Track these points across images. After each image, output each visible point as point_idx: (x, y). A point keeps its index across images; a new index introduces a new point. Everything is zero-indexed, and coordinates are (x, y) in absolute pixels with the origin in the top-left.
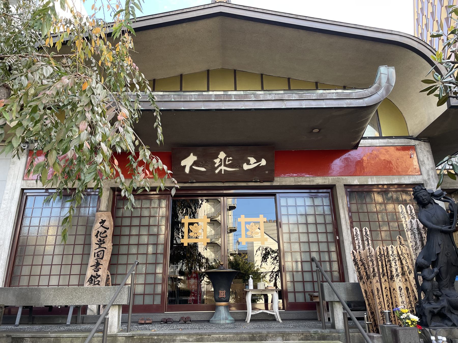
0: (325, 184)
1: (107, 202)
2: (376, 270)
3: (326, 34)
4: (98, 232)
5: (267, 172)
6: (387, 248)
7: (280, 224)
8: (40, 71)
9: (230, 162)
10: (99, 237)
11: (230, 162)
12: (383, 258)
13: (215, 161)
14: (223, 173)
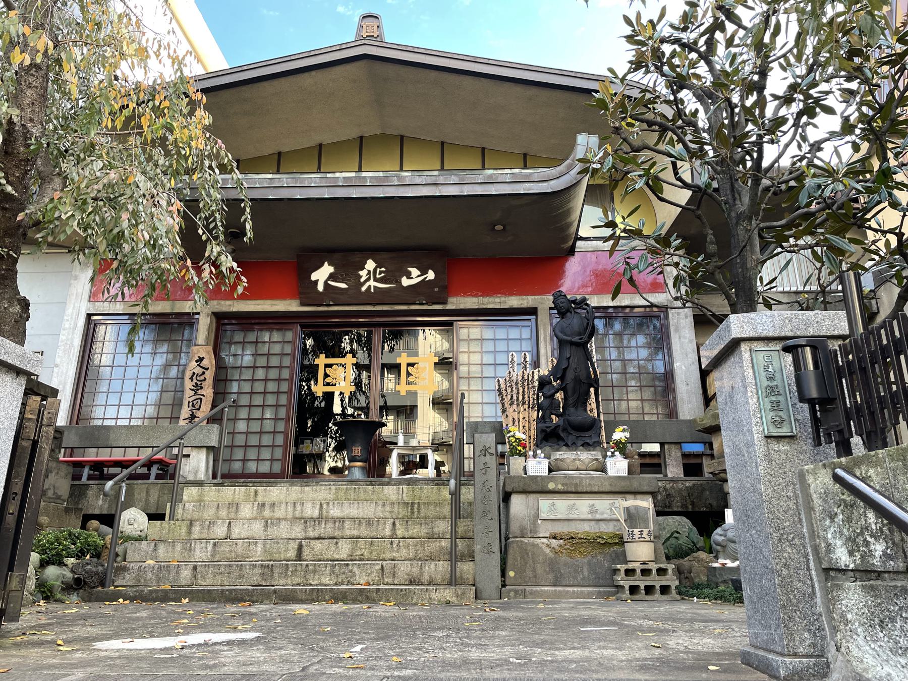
0: (522, 306)
1: (206, 333)
2: (515, 398)
3: (519, 85)
4: (194, 373)
5: (436, 290)
6: (533, 372)
7: (456, 365)
8: (90, 166)
9: (383, 275)
10: (195, 381)
11: (383, 275)
12: (526, 384)
13: (361, 273)
14: (372, 291)
